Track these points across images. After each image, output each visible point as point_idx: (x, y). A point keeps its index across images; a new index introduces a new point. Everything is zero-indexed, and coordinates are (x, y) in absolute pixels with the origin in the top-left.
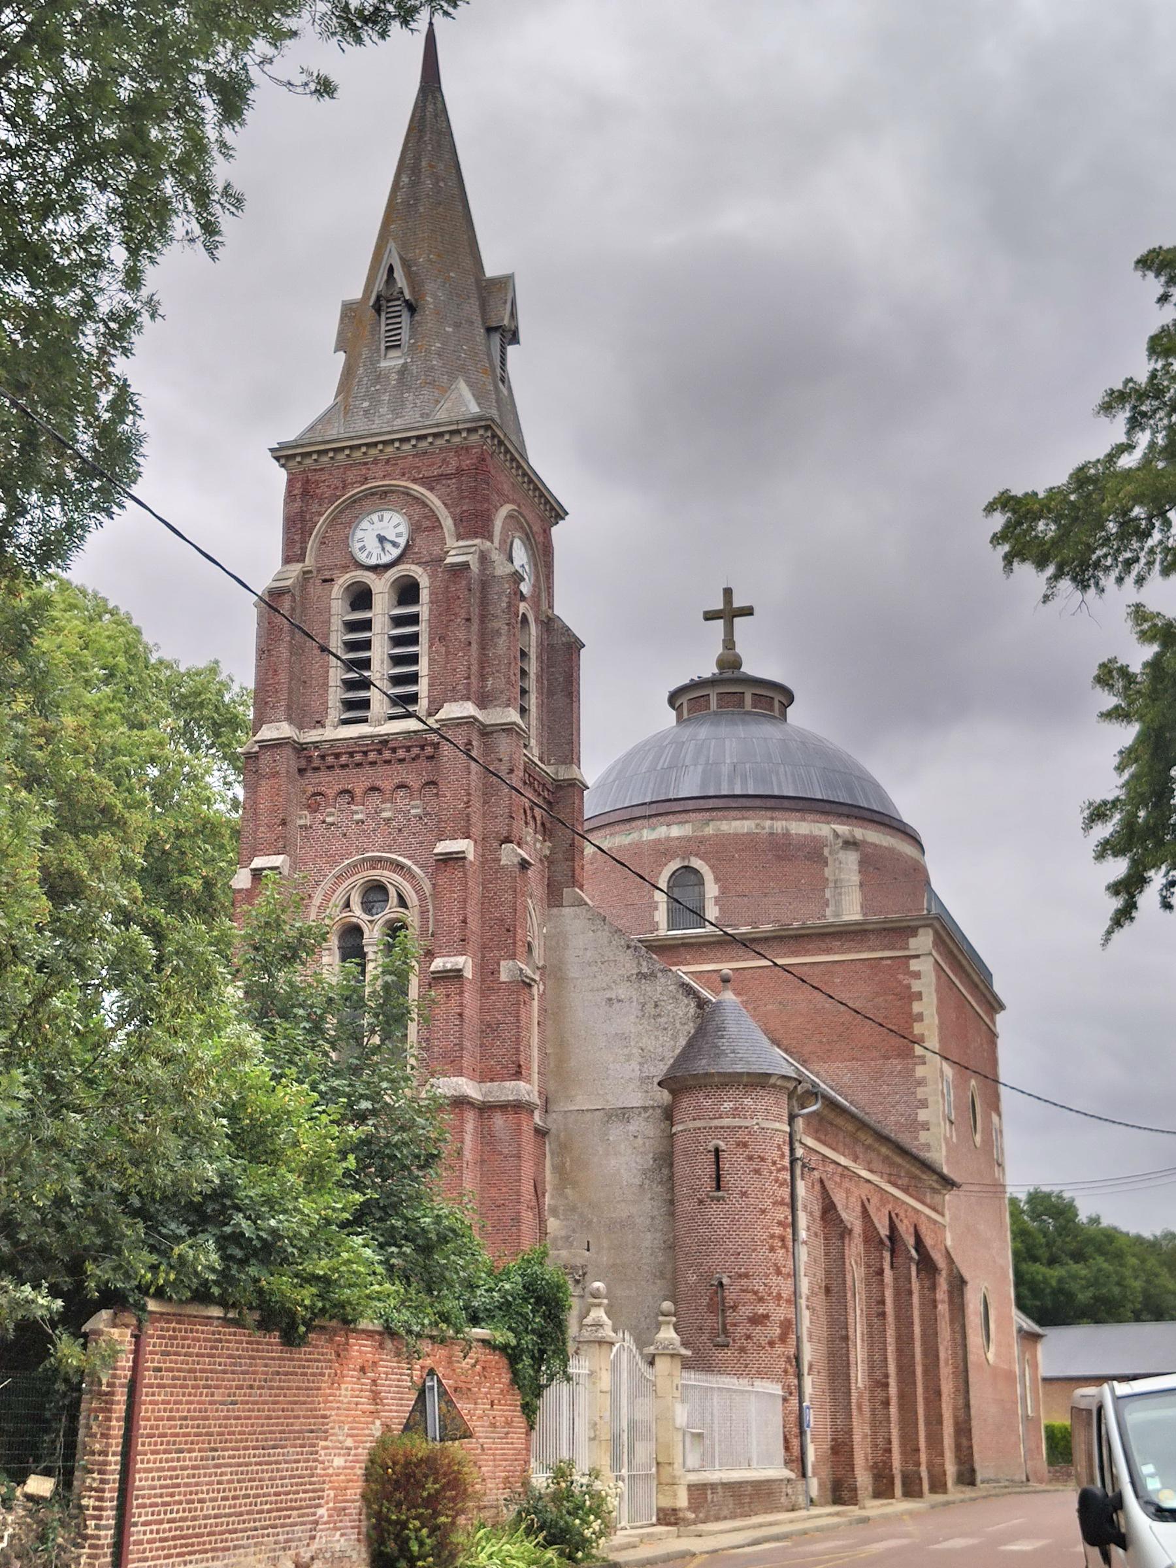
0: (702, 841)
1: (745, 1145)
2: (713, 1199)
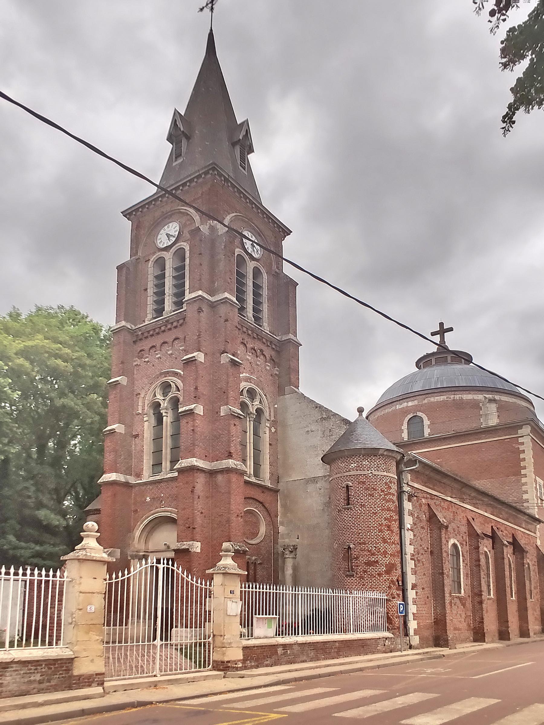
0: (422, 406)
1: (364, 483)
2: (345, 509)
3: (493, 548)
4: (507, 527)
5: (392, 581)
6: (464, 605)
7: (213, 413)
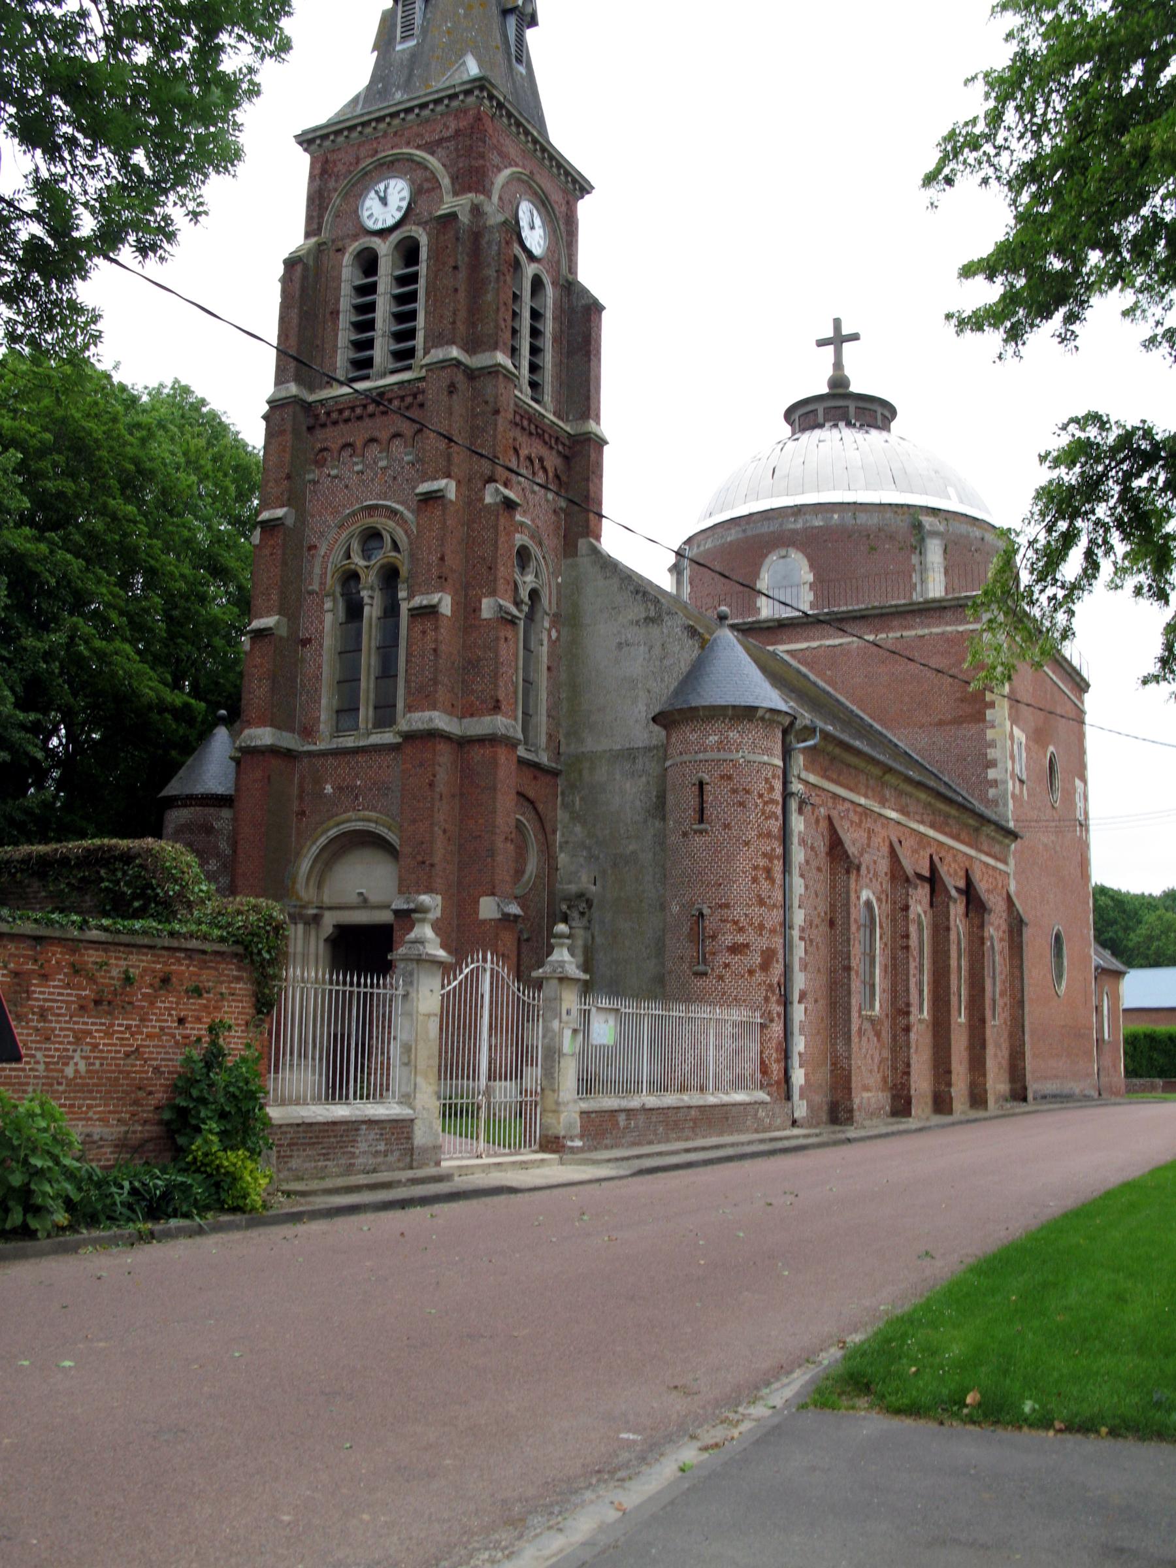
1: (730, 778)
3: (931, 905)
4: (959, 853)
5: (770, 986)
6: (878, 1034)
7: (468, 609)
